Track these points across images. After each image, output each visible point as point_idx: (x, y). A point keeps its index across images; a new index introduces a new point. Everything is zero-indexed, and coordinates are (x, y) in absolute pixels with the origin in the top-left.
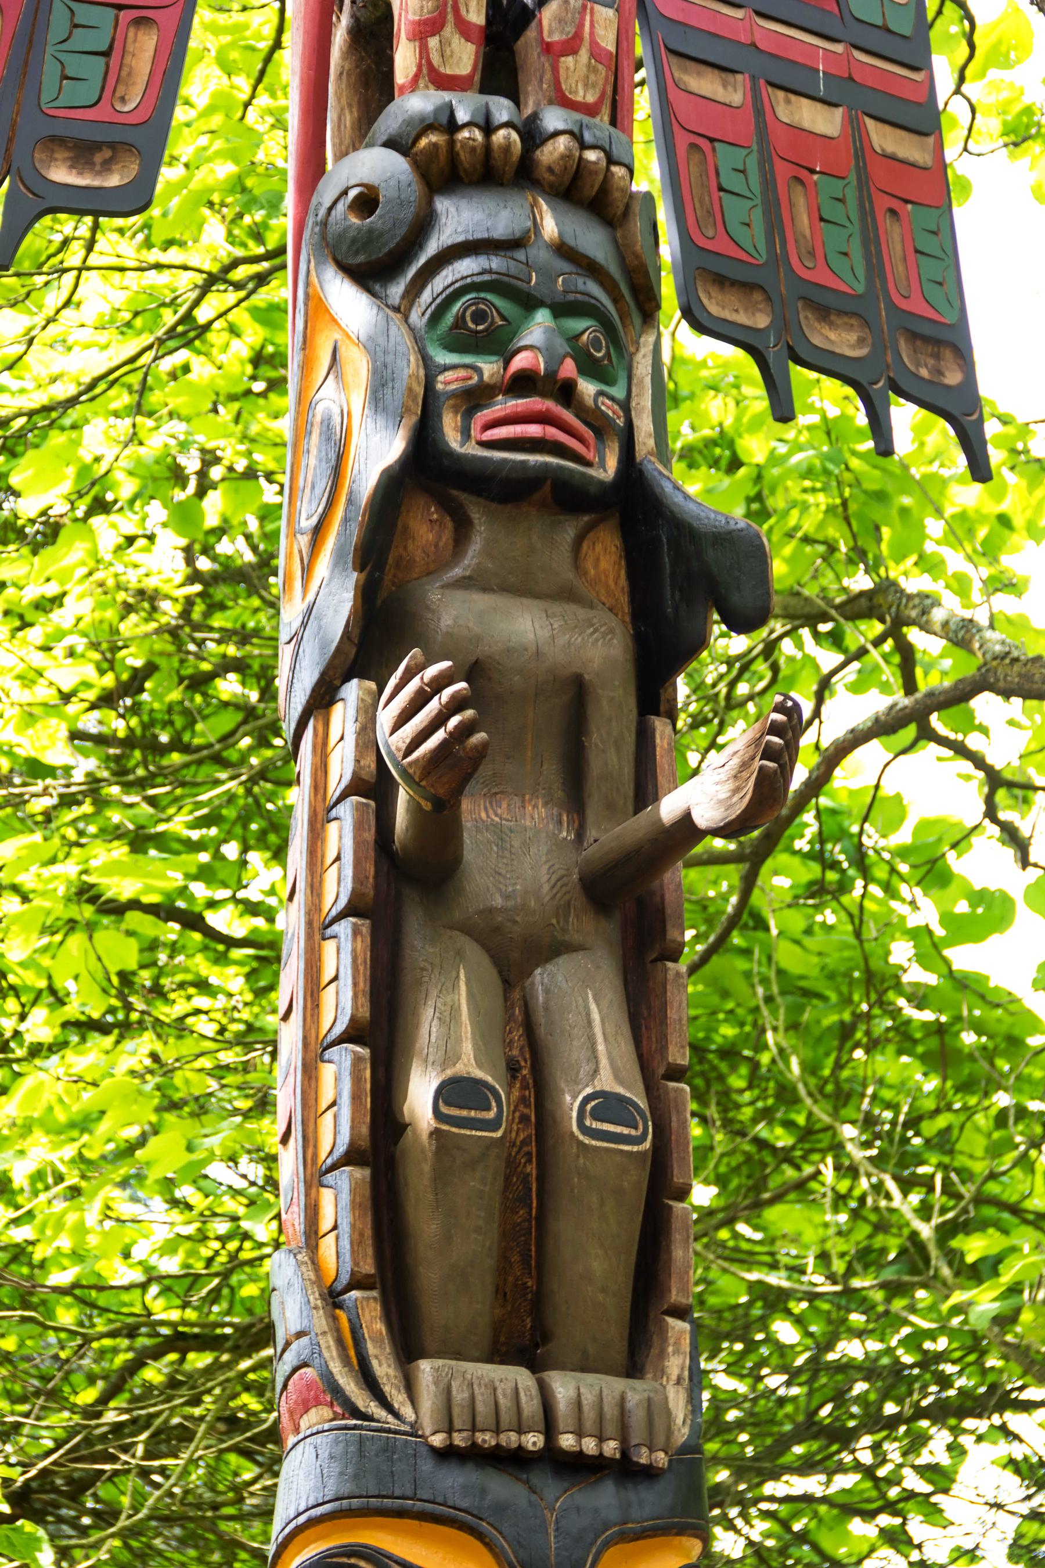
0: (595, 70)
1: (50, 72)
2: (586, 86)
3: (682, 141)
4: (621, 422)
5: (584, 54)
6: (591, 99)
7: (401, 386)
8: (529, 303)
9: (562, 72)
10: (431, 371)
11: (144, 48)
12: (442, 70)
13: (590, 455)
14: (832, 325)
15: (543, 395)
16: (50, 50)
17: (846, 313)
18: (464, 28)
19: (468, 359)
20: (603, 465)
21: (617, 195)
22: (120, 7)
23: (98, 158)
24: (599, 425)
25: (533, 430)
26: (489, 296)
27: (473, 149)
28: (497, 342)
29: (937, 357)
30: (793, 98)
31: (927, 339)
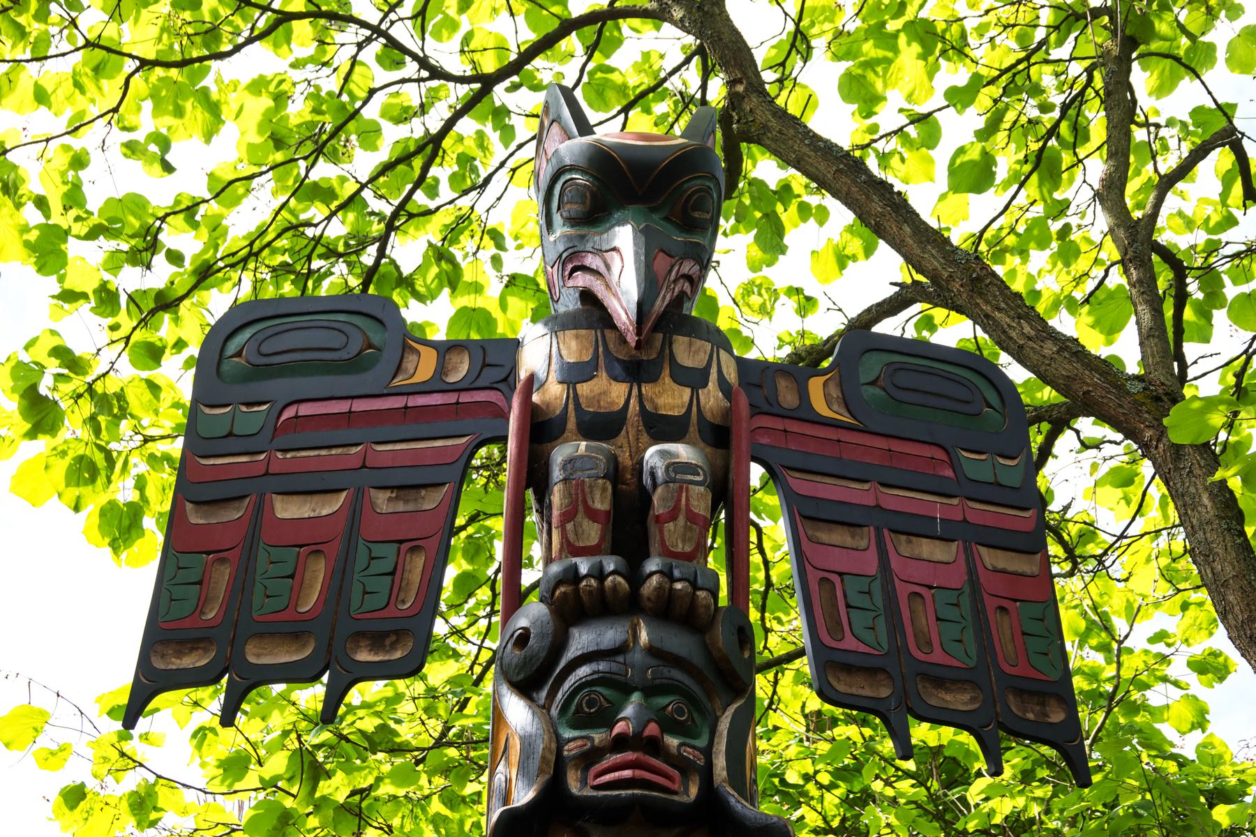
0: (691, 529)
1: (357, 589)
2: (684, 541)
3: (814, 577)
4: (701, 763)
5: (681, 520)
6: (688, 549)
7: (538, 756)
8: (626, 690)
9: (666, 533)
10: (560, 743)
11: (417, 566)
12: (577, 544)
13: (675, 787)
14: (948, 690)
15: (634, 750)
16: (356, 576)
17: (959, 681)
18: (592, 515)
19: (584, 733)
20: (687, 792)
21: (702, 610)
22: (401, 542)
23: (388, 642)
24: (684, 767)
25: (627, 773)
26: (598, 689)
27: (590, 592)
28: (606, 718)
29: (1043, 704)
30: (914, 539)
31: (1032, 693)
